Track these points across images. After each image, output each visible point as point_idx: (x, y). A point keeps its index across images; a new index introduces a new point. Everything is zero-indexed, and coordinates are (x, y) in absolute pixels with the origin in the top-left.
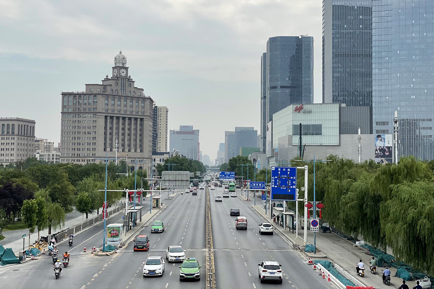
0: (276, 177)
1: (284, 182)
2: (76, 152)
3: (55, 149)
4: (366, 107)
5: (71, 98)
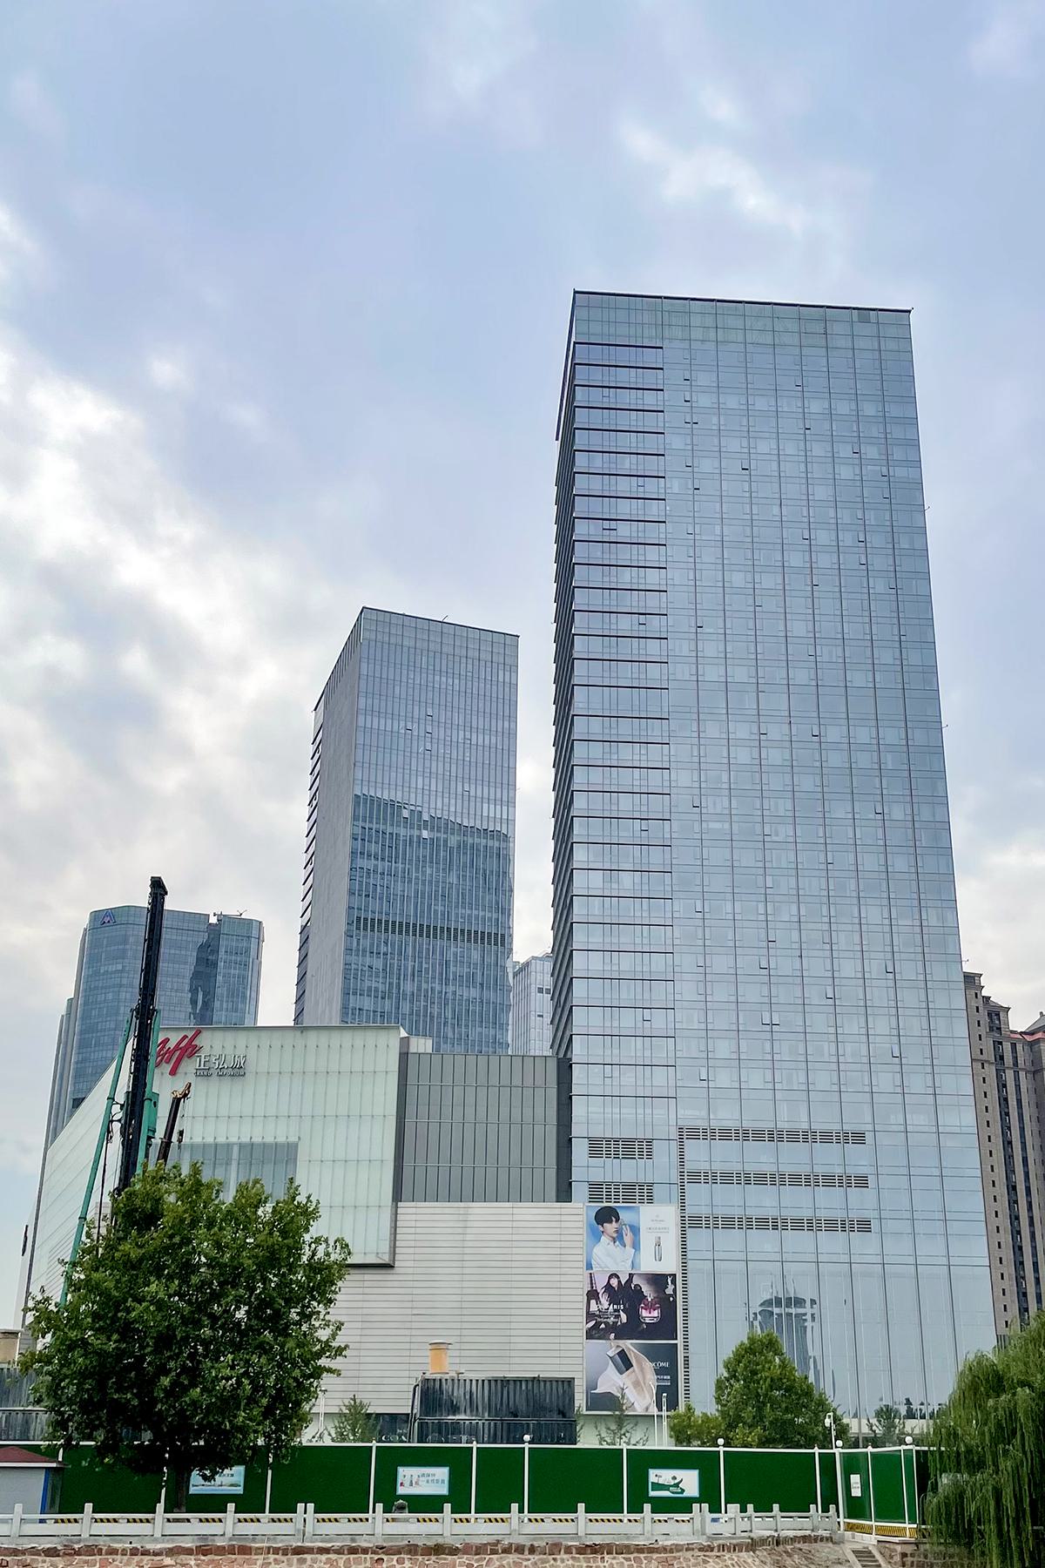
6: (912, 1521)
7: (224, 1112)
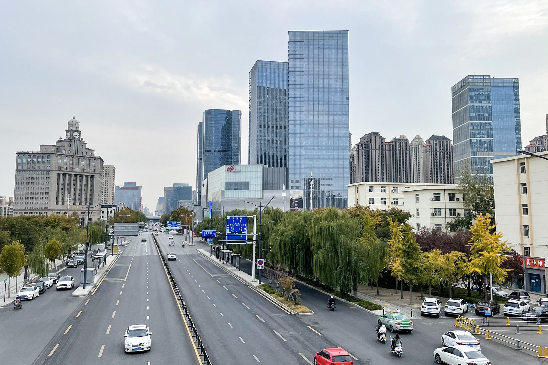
1: (237, 229)
2: (29, 206)
3: (7, 203)
5: (25, 157)
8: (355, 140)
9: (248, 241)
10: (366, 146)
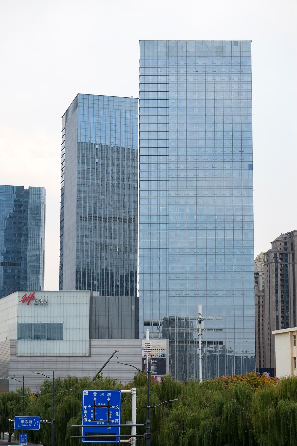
0: (90, 406)
4: (130, 298)
6: (227, 355)
7: (43, 315)
8: (262, 245)
9: (122, 438)
10: (284, 256)
